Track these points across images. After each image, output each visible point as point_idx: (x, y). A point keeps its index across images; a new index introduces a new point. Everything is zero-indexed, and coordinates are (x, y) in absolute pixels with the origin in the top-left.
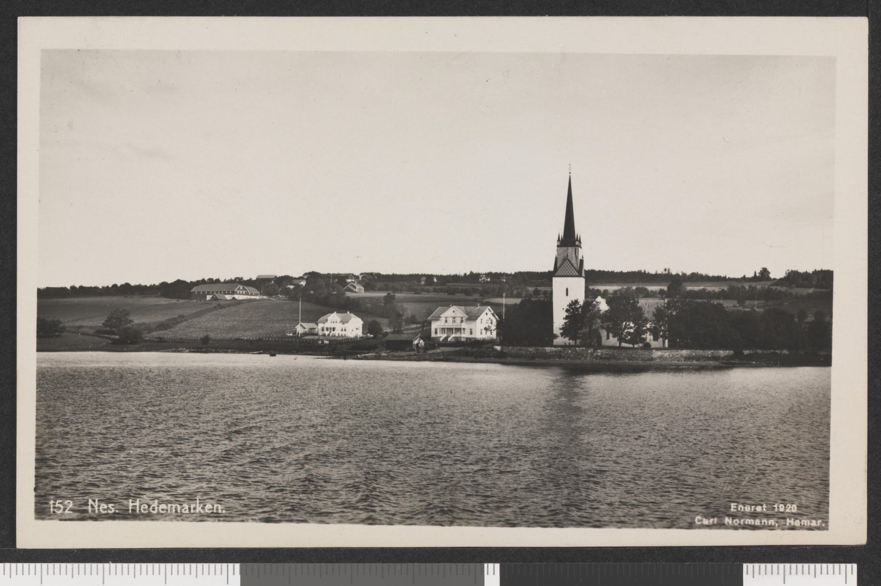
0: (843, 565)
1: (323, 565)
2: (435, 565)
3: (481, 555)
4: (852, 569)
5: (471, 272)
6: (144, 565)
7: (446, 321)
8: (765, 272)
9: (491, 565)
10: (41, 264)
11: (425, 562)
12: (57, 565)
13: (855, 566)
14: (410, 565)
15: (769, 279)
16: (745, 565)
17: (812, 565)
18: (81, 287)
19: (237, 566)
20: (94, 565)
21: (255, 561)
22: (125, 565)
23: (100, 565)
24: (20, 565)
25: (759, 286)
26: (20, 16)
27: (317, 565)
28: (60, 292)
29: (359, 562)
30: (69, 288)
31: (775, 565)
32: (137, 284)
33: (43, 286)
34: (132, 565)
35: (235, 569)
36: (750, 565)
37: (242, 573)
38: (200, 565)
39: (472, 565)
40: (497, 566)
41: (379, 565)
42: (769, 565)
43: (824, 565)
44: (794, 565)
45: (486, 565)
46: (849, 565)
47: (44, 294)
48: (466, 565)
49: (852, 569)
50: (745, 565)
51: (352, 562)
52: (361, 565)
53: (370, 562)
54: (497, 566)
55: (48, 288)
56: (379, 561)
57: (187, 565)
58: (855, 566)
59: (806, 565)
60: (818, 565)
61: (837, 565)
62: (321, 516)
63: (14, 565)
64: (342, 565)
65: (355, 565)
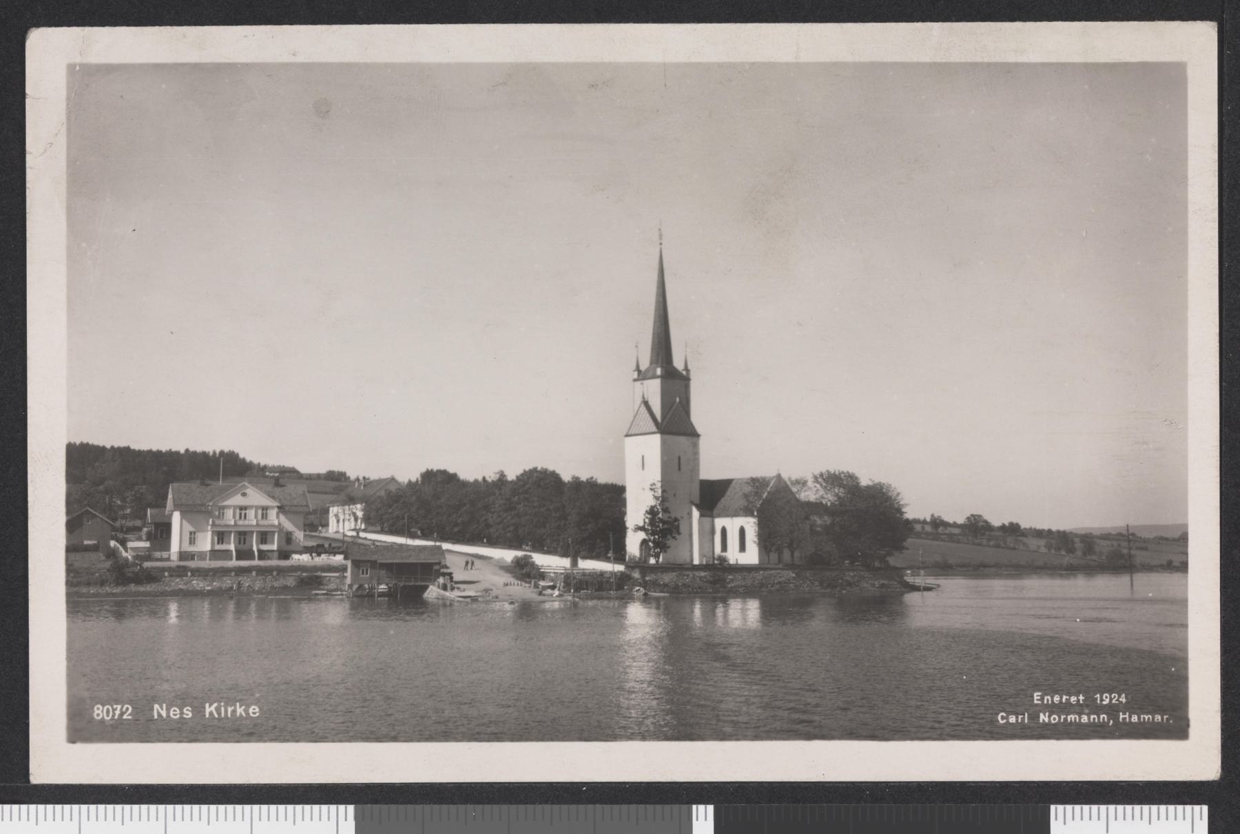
0: (1188, 808)
4: (1200, 814)
5: (187, 450)
6: (222, 807)
9: (701, 807)
10: (54, 423)
13: (1205, 808)
16: (1053, 807)
19: (351, 808)
21: (376, 802)
24: (50, 807)
30: (182, 451)
34: (204, 807)
35: (344, 818)
36: (1060, 807)
38: (299, 807)
40: (711, 808)
41: (548, 807)
43: (1163, 808)
44: (1120, 808)
45: (694, 807)
46: (1197, 808)
47: (80, 459)
49: (1200, 814)
50: (1053, 807)
51: (511, 803)
54: (711, 808)
56: (547, 802)
58: (1205, 808)
59: (1137, 808)
61: (1180, 808)
63: (41, 807)
64: (496, 807)
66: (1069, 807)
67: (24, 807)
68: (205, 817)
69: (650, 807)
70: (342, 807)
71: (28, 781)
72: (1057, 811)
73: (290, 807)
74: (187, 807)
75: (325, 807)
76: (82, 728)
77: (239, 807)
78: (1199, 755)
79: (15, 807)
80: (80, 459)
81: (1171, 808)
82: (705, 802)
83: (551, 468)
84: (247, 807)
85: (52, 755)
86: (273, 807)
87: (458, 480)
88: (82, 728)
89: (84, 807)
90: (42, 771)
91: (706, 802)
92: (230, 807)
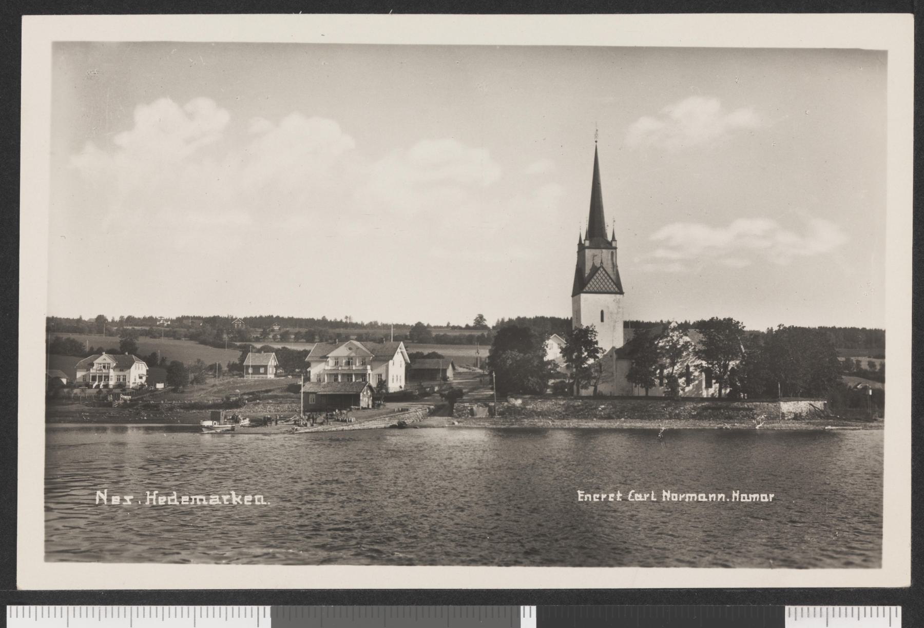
0: (887, 608)
1: (356, 607)
2: (470, 607)
3: (517, 597)
4: (895, 613)
5: (122, 317)
6: (173, 608)
7: (336, 363)
8: (480, 319)
9: (527, 608)
10: (43, 295)
11: (461, 604)
12: (84, 607)
13: (899, 608)
14: (445, 607)
15: (486, 327)
16: (787, 608)
17: (856, 608)
18: (278, 317)
19: (268, 608)
20: (122, 608)
21: (286, 603)
22: (154, 607)
23: (128, 608)
24: (46, 607)
25: (477, 333)
26: (916, 18)
27: (350, 608)
28: (77, 326)
29: (393, 604)
30: (110, 320)
31: (818, 608)
32: (75, 316)
33: (50, 316)
34: (160, 608)
35: (264, 613)
36: (793, 608)
37: (273, 615)
38: (230, 608)
39: (508, 607)
40: (534, 608)
41: (413, 607)
42: (843, 608)
43: (868, 608)
44: (837, 608)
45: (522, 607)
46: (893, 608)
47: (54, 326)
48: (502, 608)
49: (895, 613)
50: (787, 608)
51: (386, 604)
52: (394, 607)
53: (404, 604)
54: (534, 608)
55: (537, 317)
56: (413, 604)
57: (217, 608)
58: (899, 608)
59: (849, 608)
60: (862, 608)
61: (881, 608)
62: (117, 555)
63: (39, 607)
64: (375, 607)
65: (388, 608)
66: (799, 608)
67: (27, 607)
68: (115, 613)
69: (489, 607)
70: (261, 608)
71: (16, 587)
72: (11, 610)
73: (223, 607)
74: (147, 608)
75: (248, 607)
76: (56, 550)
77: (185, 607)
78: (895, 567)
79: (20, 607)
80: (54, 326)
81: (874, 608)
82: (530, 603)
83: (699, 319)
84: (192, 608)
85: (33, 569)
86: (211, 607)
87: (741, 332)
88: (56, 550)
89: (71, 607)
90: (24, 583)
91: (532, 604)
92: (179, 608)
